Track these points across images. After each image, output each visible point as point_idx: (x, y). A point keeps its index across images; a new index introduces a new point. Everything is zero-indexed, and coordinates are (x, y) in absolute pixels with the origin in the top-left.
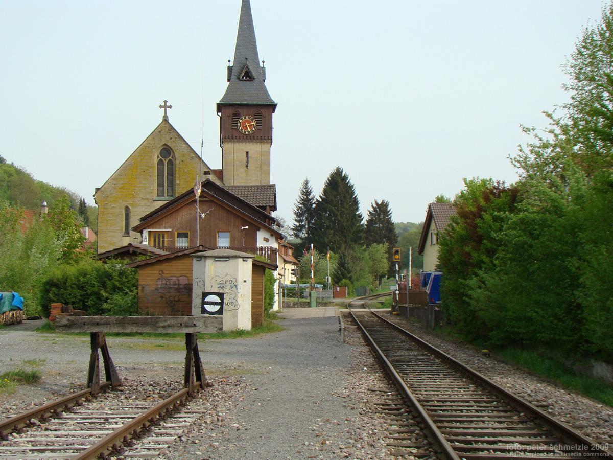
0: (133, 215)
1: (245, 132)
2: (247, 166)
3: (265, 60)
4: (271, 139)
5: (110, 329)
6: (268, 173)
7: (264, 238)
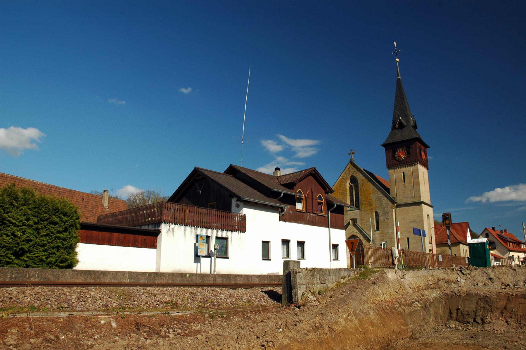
1: (400, 159)
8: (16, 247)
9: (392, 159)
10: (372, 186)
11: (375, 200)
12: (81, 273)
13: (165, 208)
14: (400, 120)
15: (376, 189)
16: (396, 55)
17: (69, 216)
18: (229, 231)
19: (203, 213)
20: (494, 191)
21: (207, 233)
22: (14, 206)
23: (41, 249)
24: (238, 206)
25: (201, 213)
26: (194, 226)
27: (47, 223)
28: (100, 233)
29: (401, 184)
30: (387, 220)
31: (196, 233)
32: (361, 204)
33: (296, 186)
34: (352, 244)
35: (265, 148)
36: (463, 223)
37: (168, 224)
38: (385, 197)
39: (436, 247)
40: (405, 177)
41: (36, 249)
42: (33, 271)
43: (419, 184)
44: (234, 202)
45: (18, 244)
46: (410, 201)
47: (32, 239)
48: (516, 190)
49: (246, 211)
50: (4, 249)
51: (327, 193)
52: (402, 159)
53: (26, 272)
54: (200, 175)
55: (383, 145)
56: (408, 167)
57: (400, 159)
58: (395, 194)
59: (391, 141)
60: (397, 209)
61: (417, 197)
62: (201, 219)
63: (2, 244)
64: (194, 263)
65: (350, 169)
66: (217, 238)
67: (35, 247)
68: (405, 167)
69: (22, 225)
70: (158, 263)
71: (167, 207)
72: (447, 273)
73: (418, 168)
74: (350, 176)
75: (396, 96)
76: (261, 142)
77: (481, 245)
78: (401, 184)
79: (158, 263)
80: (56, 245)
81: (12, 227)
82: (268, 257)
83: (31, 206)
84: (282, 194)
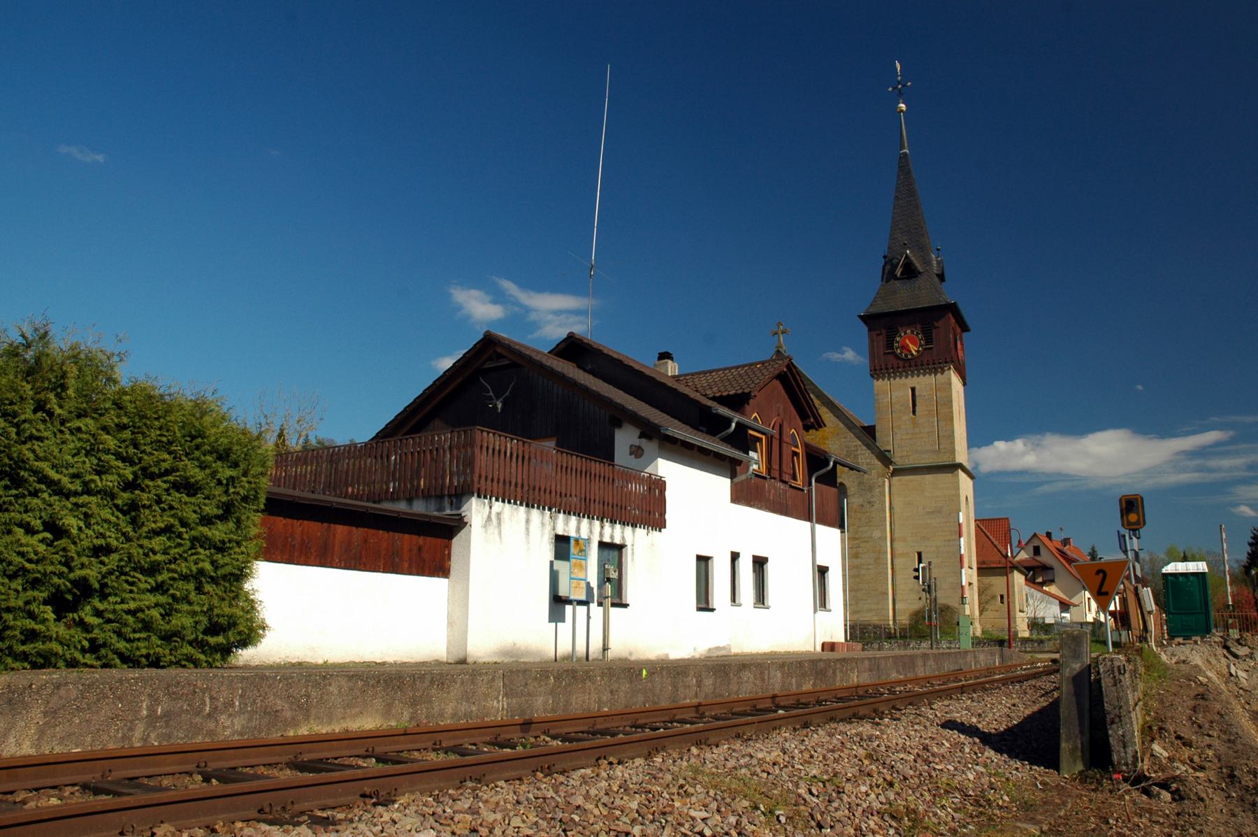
1: (906, 355)
2: (914, 412)
5: (113, 659)
7: (631, 446)
8: (61, 575)
9: (885, 354)
12: (373, 686)
13: (481, 447)
14: (907, 257)
15: (841, 425)
16: (900, 95)
17: (235, 465)
18: (628, 525)
19: (571, 470)
20: (991, 446)
21: (578, 529)
22: (50, 414)
23: (145, 582)
24: (637, 452)
25: (567, 468)
26: (550, 509)
27: (166, 486)
28: (296, 523)
30: (868, 506)
31: (554, 530)
33: (748, 404)
34: (1101, 575)
35: (460, 308)
36: (997, 519)
37: (486, 501)
38: (864, 448)
39: (979, 575)
40: (918, 401)
41: (127, 581)
42: (224, 688)
43: (952, 419)
44: (625, 438)
45: (67, 563)
46: (927, 461)
47: (115, 543)
48: (1037, 446)
49: (666, 469)
50: (20, 581)
51: (807, 428)
52: (912, 354)
53: (203, 691)
54: (500, 356)
55: (866, 319)
57: (906, 355)
58: (888, 442)
59: (874, 310)
60: (895, 479)
62: (566, 489)
63: (10, 563)
64: (550, 622)
66: (602, 545)
67: (126, 574)
69: (80, 489)
70: (458, 622)
71: (486, 445)
72: (1215, 655)
73: (950, 379)
75: (896, 197)
76: (453, 291)
77: (1195, 578)
79: (458, 622)
80: (194, 568)
81: (46, 495)
82: (707, 602)
83: (111, 419)
84: (733, 425)
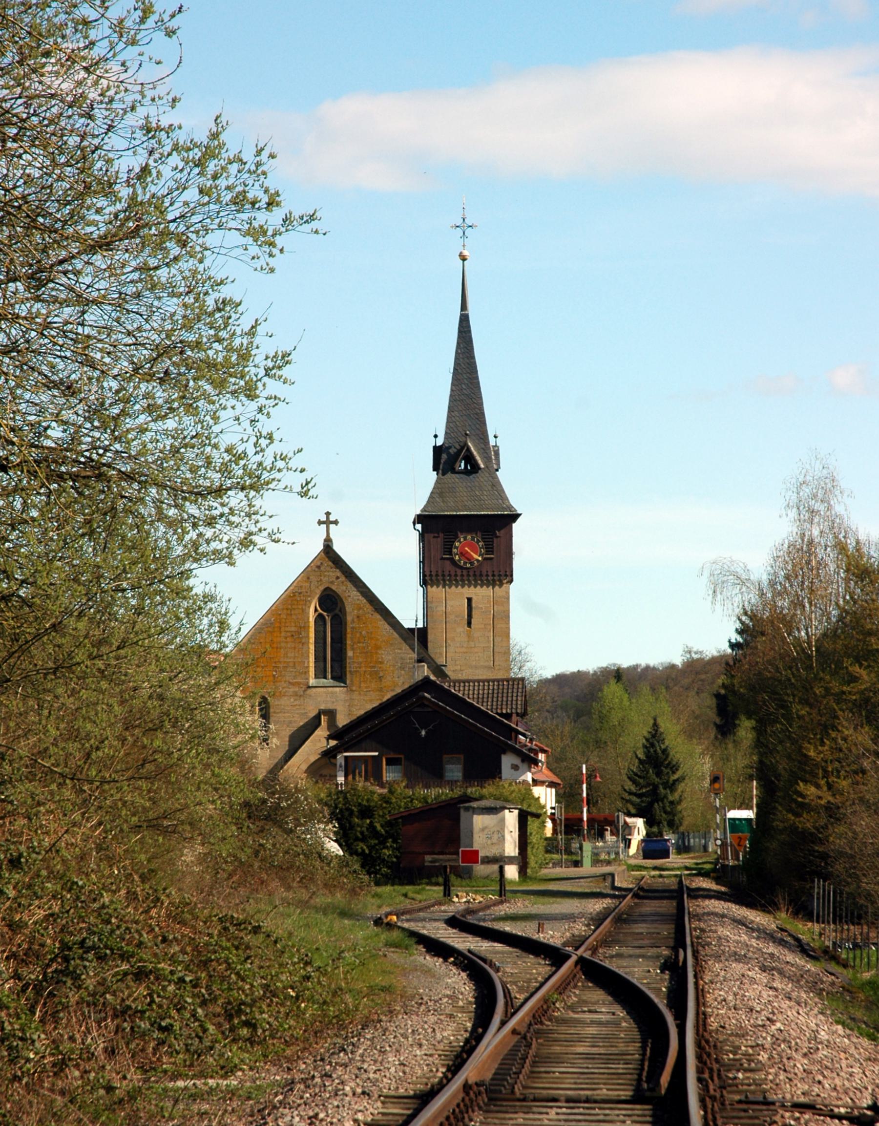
0: (275, 712)
2: (469, 624)
3: (498, 434)
4: (512, 575)
6: (437, 482)
9: (442, 559)
10: (387, 626)
11: (394, 666)
29: (462, 630)
32: (350, 671)
56: (475, 587)
58: (441, 654)
61: (499, 669)
65: (322, 568)
68: (475, 587)
74: (322, 588)
78: (462, 630)
